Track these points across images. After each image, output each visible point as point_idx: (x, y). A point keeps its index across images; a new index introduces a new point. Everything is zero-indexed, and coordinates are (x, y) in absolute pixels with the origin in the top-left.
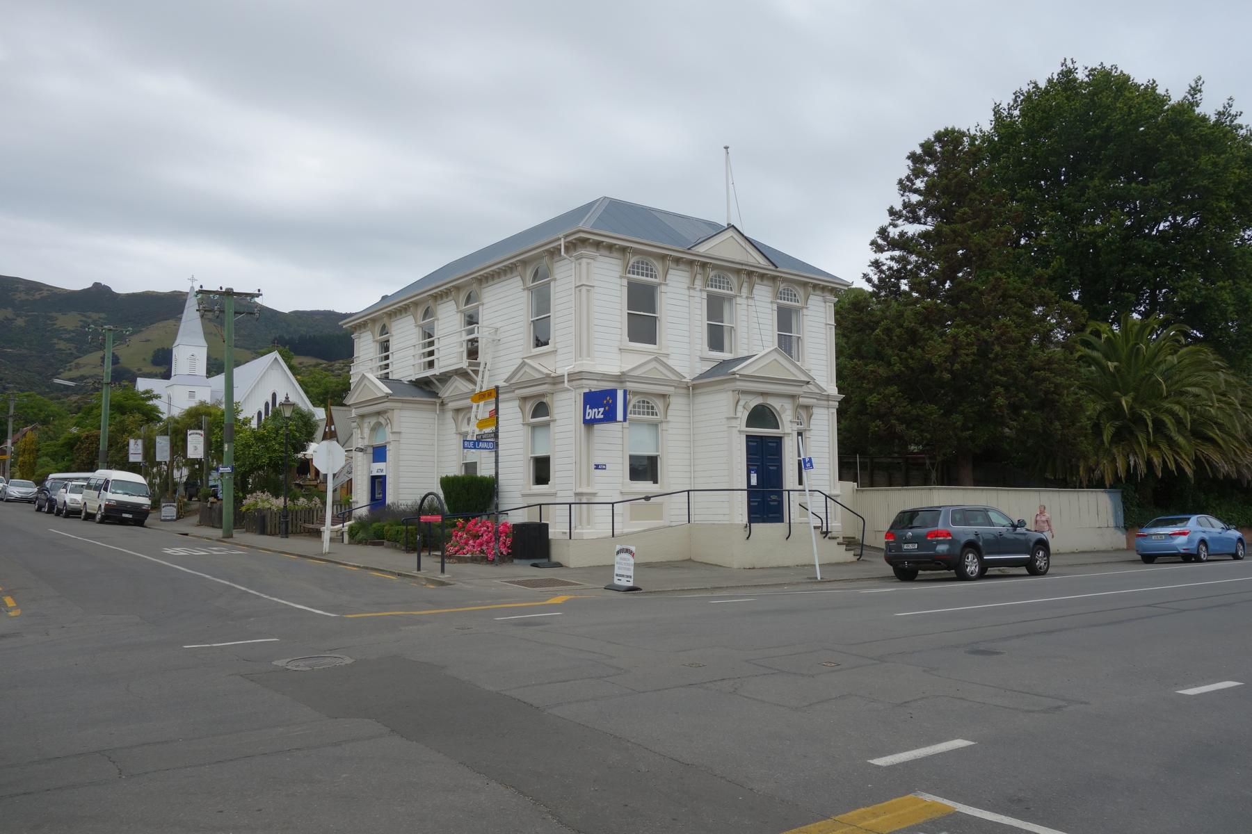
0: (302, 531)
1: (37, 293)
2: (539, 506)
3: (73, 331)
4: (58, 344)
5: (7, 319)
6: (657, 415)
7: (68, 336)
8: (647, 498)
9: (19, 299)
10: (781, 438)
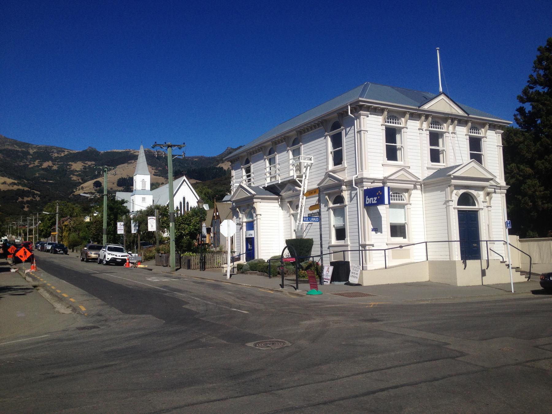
0: (197, 268)
1: (63, 153)
2: (425, 243)
3: (80, 171)
4: (73, 177)
5: (49, 166)
6: (404, 200)
7: (77, 173)
8: (401, 247)
9: (54, 157)
10: (477, 211)
